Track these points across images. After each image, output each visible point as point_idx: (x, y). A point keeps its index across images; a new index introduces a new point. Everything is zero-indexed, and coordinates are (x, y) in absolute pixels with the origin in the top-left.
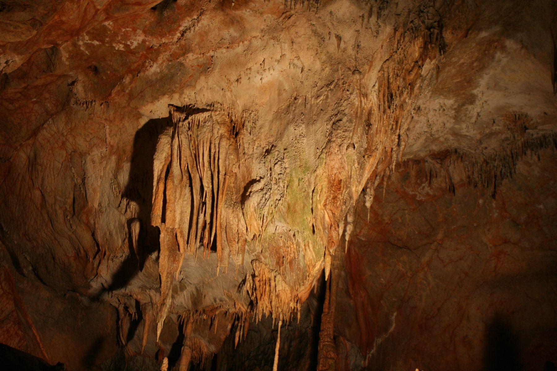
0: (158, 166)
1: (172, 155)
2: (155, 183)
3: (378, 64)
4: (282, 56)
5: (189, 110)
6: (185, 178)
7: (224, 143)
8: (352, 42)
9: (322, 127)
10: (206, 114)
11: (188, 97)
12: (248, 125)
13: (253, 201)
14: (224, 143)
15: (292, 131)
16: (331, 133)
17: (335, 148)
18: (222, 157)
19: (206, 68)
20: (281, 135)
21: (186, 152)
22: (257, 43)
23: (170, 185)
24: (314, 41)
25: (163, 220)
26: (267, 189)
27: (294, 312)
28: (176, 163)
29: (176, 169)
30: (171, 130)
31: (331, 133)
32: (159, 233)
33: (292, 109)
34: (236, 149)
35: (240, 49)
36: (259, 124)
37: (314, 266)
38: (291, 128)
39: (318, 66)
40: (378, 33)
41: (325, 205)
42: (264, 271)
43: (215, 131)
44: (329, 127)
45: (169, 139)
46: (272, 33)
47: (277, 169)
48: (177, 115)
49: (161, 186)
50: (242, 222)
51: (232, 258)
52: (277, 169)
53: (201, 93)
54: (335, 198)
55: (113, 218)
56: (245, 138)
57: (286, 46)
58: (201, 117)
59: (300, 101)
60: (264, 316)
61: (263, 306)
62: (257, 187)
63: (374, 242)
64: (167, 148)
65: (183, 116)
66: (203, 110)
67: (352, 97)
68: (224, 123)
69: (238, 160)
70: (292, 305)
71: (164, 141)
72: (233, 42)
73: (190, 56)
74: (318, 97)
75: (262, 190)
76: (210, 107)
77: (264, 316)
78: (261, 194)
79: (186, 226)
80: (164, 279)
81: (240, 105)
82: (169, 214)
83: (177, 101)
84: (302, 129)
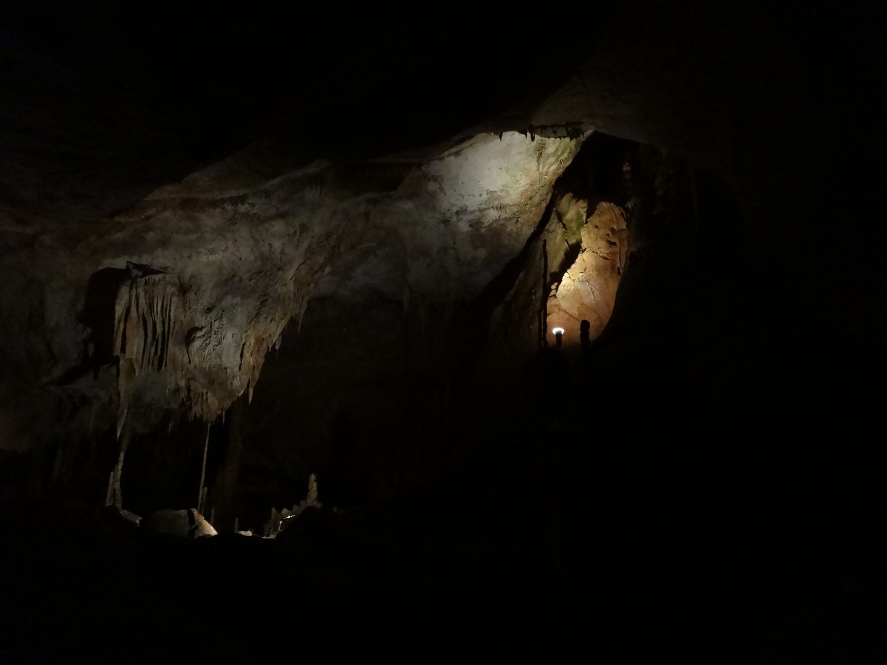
0: (119, 310)
1: (130, 302)
2: (116, 323)
3: (295, 267)
4: (227, 248)
5: (147, 270)
6: (141, 321)
7: (175, 299)
8: (280, 249)
9: (253, 303)
10: (161, 276)
11: (145, 260)
12: (194, 288)
13: (197, 344)
14: (175, 299)
15: (228, 300)
16: (260, 308)
17: (262, 318)
18: (173, 309)
19: (164, 243)
20: (219, 300)
21: (142, 301)
22: (208, 236)
23: (129, 326)
24: (251, 242)
25: (123, 350)
26: (208, 335)
27: (219, 417)
28: (133, 309)
29: (133, 313)
30: (129, 282)
31: (260, 308)
32: (119, 360)
33: (229, 283)
34: (184, 304)
35: (193, 237)
36: (203, 288)
37: (239, 392)
38: (229, 297)
39: (252, 258)
40: (298, 246)
41: (251, 355)
42: (198, 386)
43: (168, 289)
44: (258, 303)
45: (128, 289)
46: (220, 232)
47: (217, 324)
48: (135, 272)
49: (122, 325)
50: (187, 356)
51: (174, 379)
52: (217, 324)
53: (160, 259)
54: (259, 350)
55: (70, 339)
56: (191, 296)
57: (230, 243)
58: (157, 277)
59: (237, 279)
60: (195, 416)
61: (197, 410)
62: (199, 334)
63: (276, 363)
64: (126, 297)
65: (140, 274)
66: (158, 272)
67: (277, 286)
68: (174, 285)
69: (185, 311)
70: (219, 413)
71: (124, 296)
72: (188, 232)
73: (151, 234)
74: (251, 280)
75: (203, 336)
76: (163, 270)
77: (195, 416)
78: (203, 339)
79: (141, 355)
80: (122, 394)
81: (189, 272)
82: (128, 347)
83: (135, 260)
84: (237, 300)
